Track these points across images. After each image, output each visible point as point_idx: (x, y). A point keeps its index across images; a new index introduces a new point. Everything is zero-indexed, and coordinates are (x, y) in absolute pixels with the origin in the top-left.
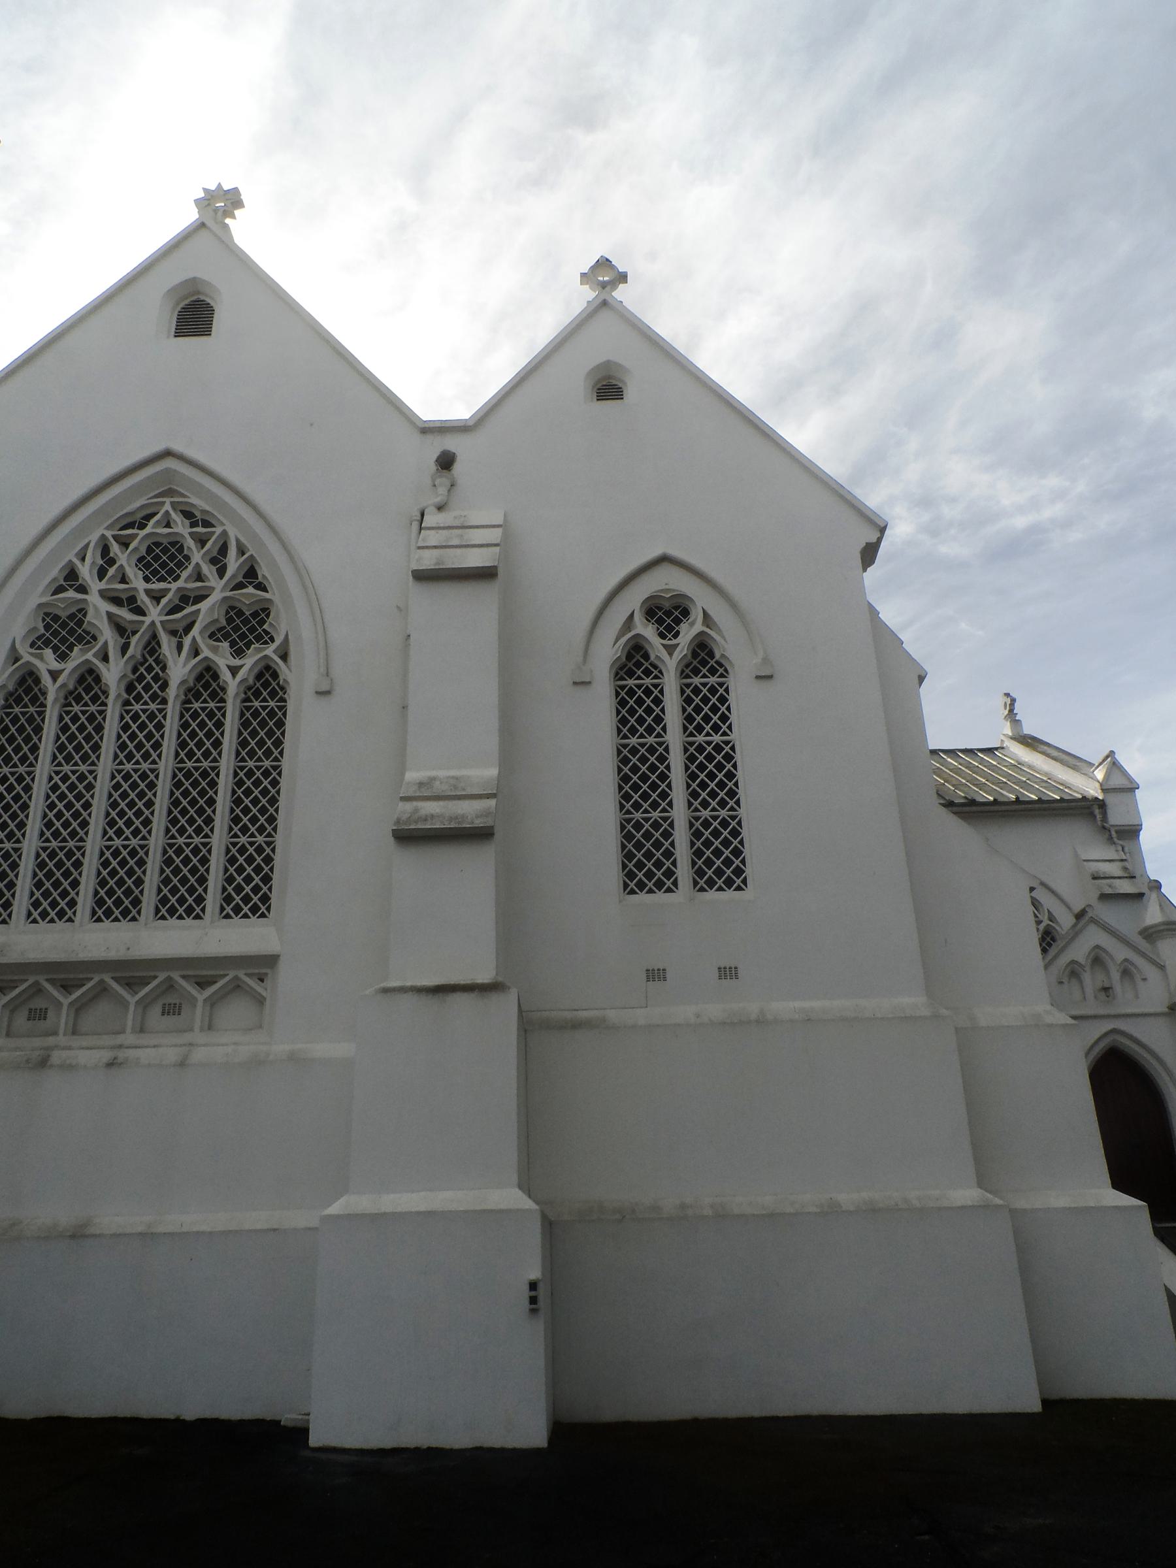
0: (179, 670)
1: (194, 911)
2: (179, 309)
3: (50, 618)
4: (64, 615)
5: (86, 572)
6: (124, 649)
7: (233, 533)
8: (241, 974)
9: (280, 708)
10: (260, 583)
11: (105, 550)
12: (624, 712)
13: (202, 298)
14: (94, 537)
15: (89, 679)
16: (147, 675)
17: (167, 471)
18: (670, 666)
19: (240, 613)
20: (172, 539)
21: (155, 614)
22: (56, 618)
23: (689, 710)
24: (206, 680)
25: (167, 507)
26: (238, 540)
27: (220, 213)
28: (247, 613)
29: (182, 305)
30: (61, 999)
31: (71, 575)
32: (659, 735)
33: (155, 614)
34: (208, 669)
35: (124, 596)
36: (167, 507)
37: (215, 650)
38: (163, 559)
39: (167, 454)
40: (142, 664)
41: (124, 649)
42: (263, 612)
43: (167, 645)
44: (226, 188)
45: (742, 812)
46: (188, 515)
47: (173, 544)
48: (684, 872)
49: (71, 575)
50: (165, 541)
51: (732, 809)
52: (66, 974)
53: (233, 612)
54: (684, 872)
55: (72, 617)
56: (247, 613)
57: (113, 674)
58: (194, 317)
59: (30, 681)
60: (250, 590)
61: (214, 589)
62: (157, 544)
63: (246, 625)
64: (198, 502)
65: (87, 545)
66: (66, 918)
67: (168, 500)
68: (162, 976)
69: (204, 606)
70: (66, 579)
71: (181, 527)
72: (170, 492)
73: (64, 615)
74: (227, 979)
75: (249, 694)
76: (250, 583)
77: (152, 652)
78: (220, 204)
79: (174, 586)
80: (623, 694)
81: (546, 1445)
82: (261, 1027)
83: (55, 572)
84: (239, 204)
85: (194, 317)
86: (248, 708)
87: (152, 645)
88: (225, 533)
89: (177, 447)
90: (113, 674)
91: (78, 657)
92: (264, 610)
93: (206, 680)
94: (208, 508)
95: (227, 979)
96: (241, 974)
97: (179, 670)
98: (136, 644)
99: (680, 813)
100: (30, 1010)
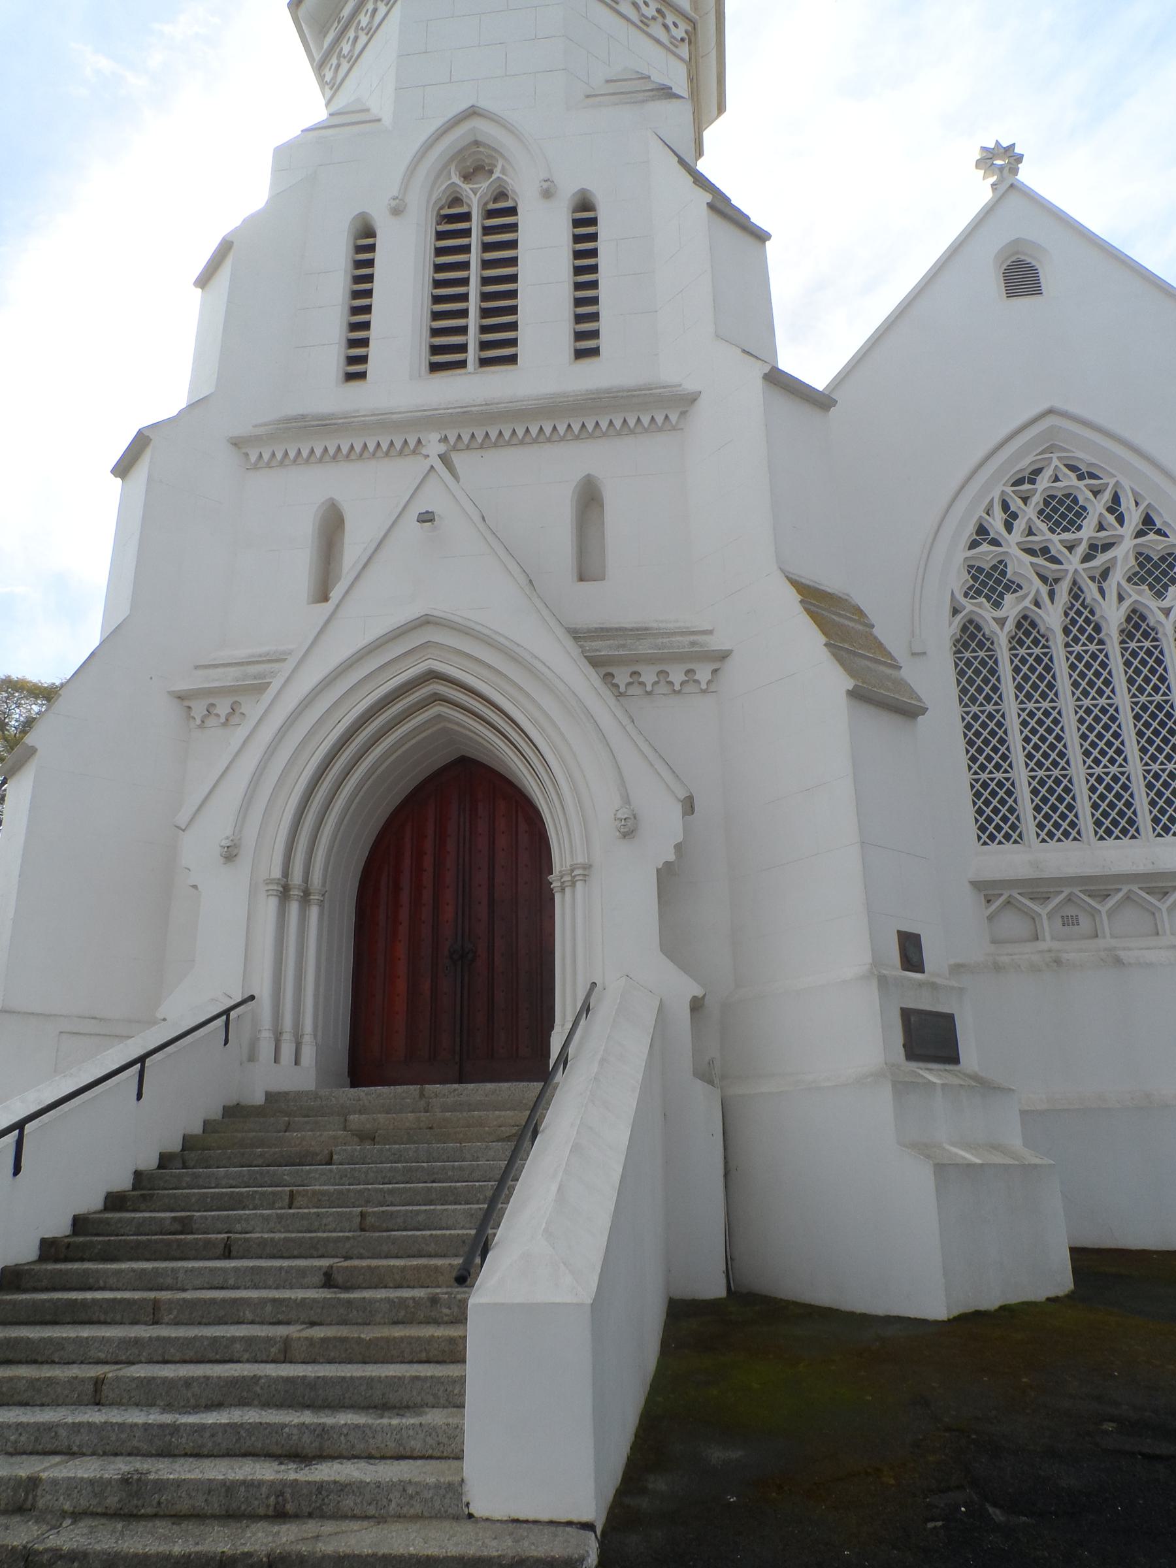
0: (1113, 616)
1: (1071, 832)
2: (1005, 267)
3: (975, 571)
4: (987, 567)
5: (996, 523)
6: (1052, 594)
7: (1126, 484)
8: (1135, 888)
10: (1159, 530)
11: (1005, 506)
12: (963, 681)
13: (1023, 258)
14: (996, 495)
15: (1027, 626)
18: (1002, 640)
19: (1148, 559)
21: (1073, 563)
22: (980, 570)
23: (993, 680)
25: (1055, 462)
26: (1132, 490)
27: (1006, 171)
28: (1156, 559)
31: (982, 530)
33: (1073, 563)
35: (1037, 548)
37: (1140, 593)
38: (1063, 512)
39: (1051, 411)
40: (1071, 609)
41: (1052, 594)
43: (1091, 591)
44: (1005, 145)
45: (967, 777)
47: (1068, 496)
48: (1029, 824)
49: (982, 530)
50: (1059, 494)
51: (1063, 769)
52: (1099, 887)
54: (1029, 824)
55: (994, 568)
56: (1156, 559)
57: (1052, 618)
58: (1021, 278)
59: (972, 628)
61: (1122, 537)
62: (1053, 497)
64: (1084, 458)
65: (992, 500)
67: (1054, 456)
68: (1066, 891)
69: (1117, 552)
70: (977, 534)
71: (1070, 480)
72: (1051, 449)
73: (987, 567)
74: (1120, 895)
75: (959, 646)
78: (1001, 161)
79: (1049, 535)
80: (961, 664)
81: (1072, 1286)
82: (1097, 936)
84: (1019, 158)
85: (1021, 278)
86: (960, 659)
87: (1076, 592)
89: (1059, 405)
90: (1052, 618)
91: (1012, 607)
95: (1120, 895)
96: (1135, 888)
97: (1113, 616)
98: (1063, 589)
99: (1135, 767)
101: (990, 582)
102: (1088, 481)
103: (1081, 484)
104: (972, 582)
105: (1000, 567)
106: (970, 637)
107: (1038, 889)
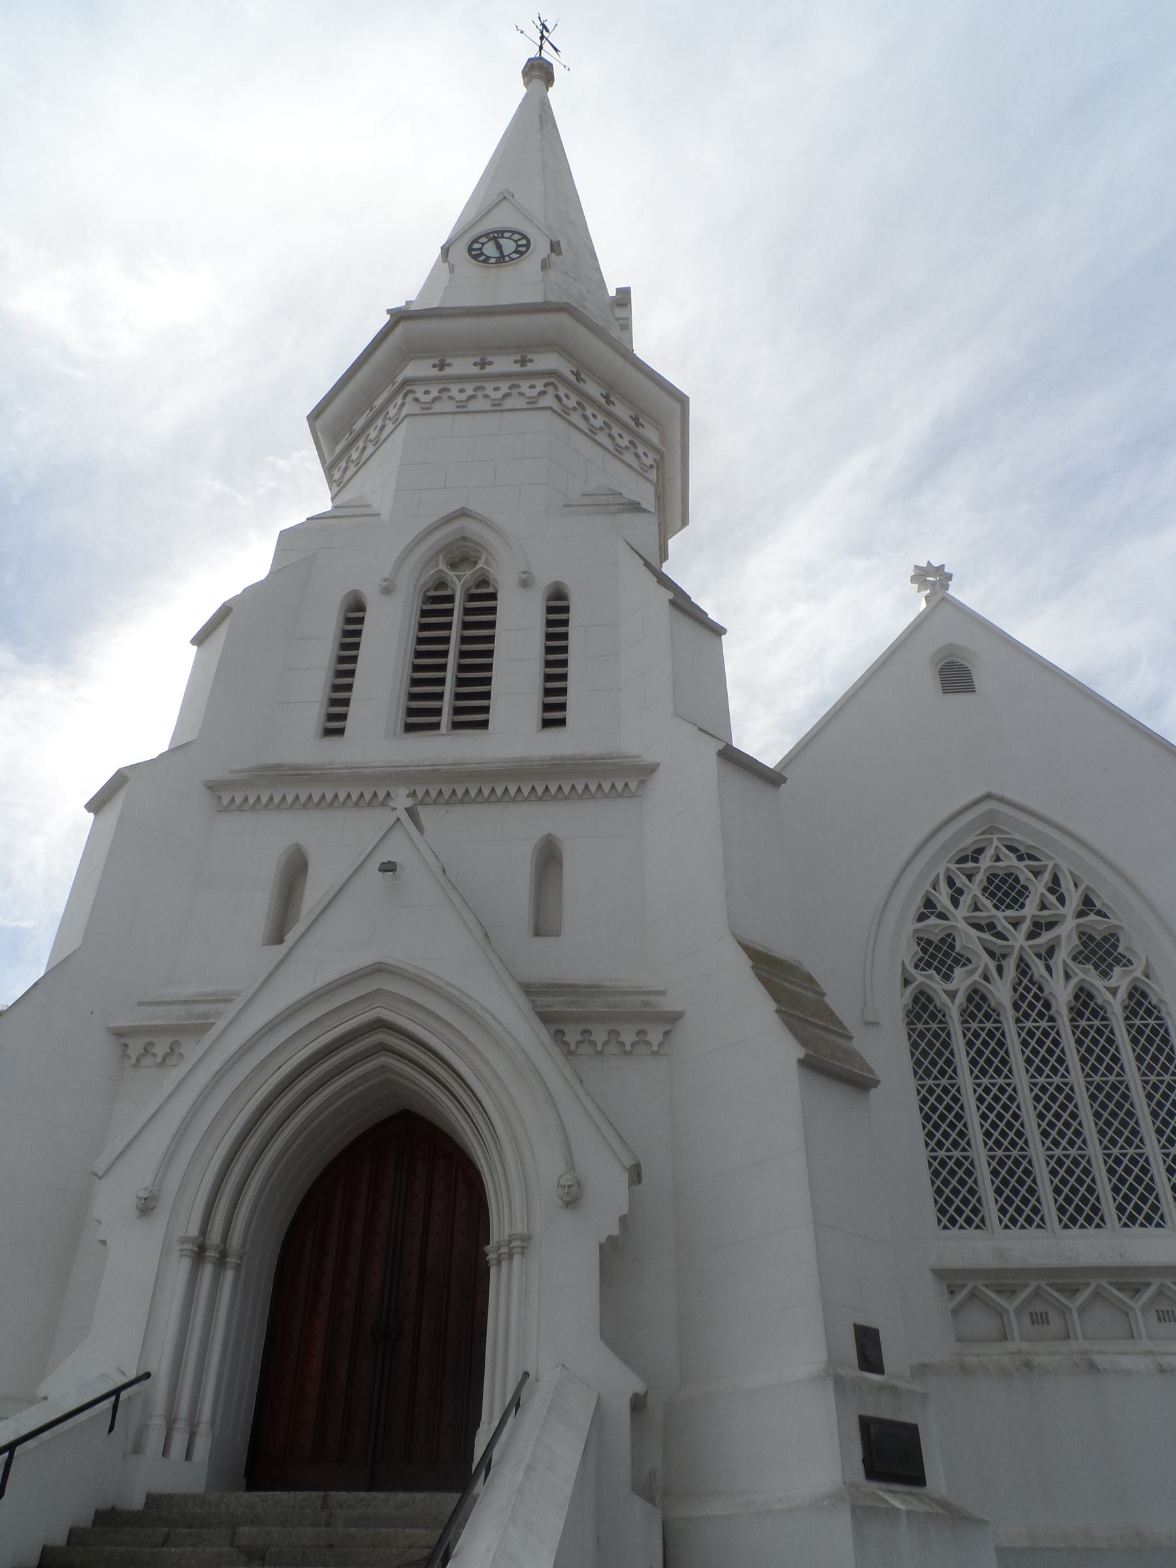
0: (1061, 994)
1: (1033, 1219)
3: (924, 943)
7: (1064, 866)
9: (943, 1030)
11: (951, 882)
13: (956, 660)
14: (941, 870)
15: (977, 1000)
16: (1032, 999)
17: (991, 811)
20: (1007, 871)
23: (947, 1053)
24: (1083, 1000)
25: (996, 843)
29: (940, 666)
30: (1004, 1304)
31: (929, 904)
32: (923, 1086)
34: (922, 993)
36: (996, 843)
37: (1086, 972)
38: (1007, 891)
39: (989, 796)
42: (1111, 939)
43: (1038, 968)
46: (1013, 849)
49: (929, 904)
50: (1001, 873)
52: (1068, 1280)
53: (1086, 938)
55: (943, 941)
57: (1002, 993)
58: (955, 676)
60: (933, 920)
63: (1101, 951)
66: (1035, 1224)
67: (995, 837)
71: (1010, 860)
72: (991, 830)
76: (932, 913)
77: (1024, 973)
79: (994, 912)
83: (917, 903)
87: (1023, 968)
88: (1056, 866)
89: (995, 790)
90: (1002, 993)
92: (949, 935)
93: (1083, 1000)
94: (1033, 844)
97: (1061, 994)
98: (1010, 965)
100: (1031, 1314)
101: (938, 954)
102: (1028, 862)
103: (1021, 865)
104: (921, 954)
105: (948, 940)
106: (922, 1008)
107: (1005, 1281)
